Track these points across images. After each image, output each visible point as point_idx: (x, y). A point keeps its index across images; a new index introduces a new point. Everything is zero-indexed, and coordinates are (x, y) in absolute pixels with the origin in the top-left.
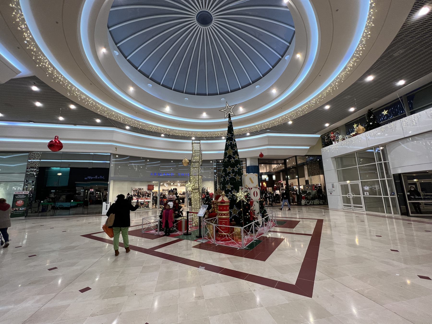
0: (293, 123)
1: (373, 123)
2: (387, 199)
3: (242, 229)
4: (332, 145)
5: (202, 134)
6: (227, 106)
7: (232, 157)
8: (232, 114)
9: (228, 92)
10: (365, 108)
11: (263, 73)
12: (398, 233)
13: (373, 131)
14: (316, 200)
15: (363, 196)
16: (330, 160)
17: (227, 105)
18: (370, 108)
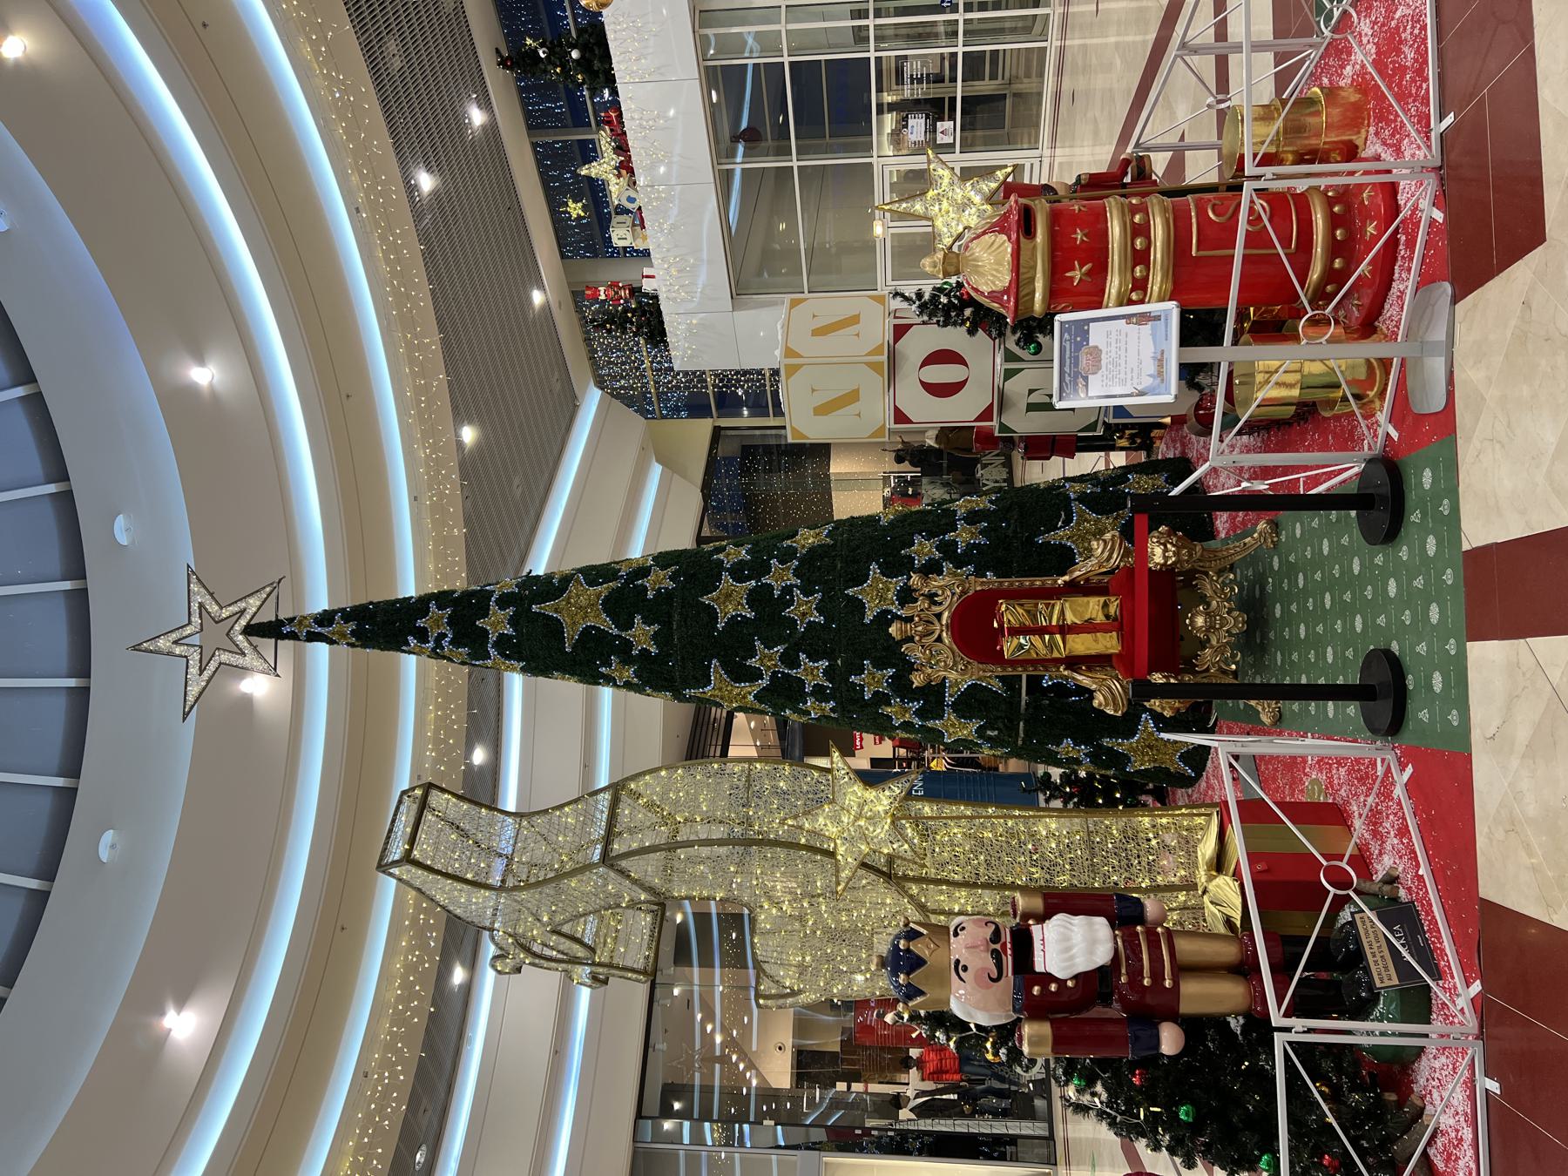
0: (470, 423)
1: (574, 47)
2: (972, 33)
3: (1260, 184)
4: (662, 298)
5: (364, 1133)
6: (176, 642)
7: (627, 582)
8: (254, 602)
9: (67, 799)
10: (486, 75)
11: (63, 662)
12: (1144, 41)
13: (615, 39)
14: (979, 475)
15: (957, 155)
16: (742, 316)
17: (162, 643)
18: (494, 59)
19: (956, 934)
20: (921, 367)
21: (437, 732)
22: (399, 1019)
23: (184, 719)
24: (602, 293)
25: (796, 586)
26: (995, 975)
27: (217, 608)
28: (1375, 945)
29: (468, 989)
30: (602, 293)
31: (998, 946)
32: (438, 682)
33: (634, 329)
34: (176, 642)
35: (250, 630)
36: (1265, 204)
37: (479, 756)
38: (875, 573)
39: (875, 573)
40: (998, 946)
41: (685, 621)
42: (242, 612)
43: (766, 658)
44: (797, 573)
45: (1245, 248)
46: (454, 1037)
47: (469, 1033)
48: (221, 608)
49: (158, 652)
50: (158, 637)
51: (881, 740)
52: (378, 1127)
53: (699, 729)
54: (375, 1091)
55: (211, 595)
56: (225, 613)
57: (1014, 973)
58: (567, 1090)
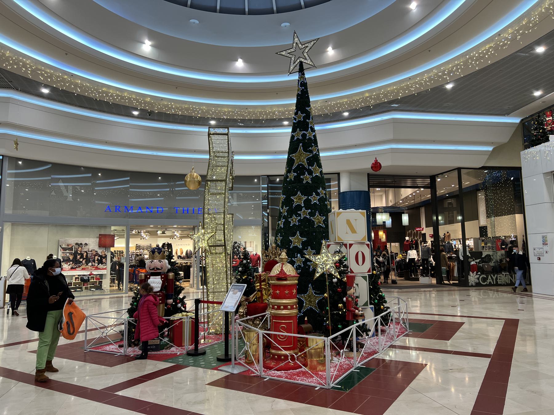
6: (297, 43)
8: (309, 62)
14: (503, 273)
19: (159, 261)
20: (362, 252)
21: (340, 103)
22: (261, 113)
23: (276, 53)
24: (549, 118)
25: (301, 217)
26: (150, 269)
27: (307, 51)
28: (152, 342)
29: (282, 126)
30: (549, 118)
31: (155, 269)
32: (354, 100)
33: (535, 134)
34: (297, 43)
35: (301, 63)
36: (52, 296)
37: (346, 114)
38: (303, 239)
39: (303, 239)
40: (155, 269)
41: (294, 188)
42: (306, 59)
43: (284, 211)
44: (305, 218)
45: (293, 336)
46: (272, 125)
47: (275, 128)
48: (307, 53)
49: (294, 39)
50: (298, 38)
51: (431, 237)
52: (234, 116)
53: (392, 177)
54: (243, 112)
55: (311, 48)
56: (305, 54)
57: (151, 272)
58: (271, 156)
